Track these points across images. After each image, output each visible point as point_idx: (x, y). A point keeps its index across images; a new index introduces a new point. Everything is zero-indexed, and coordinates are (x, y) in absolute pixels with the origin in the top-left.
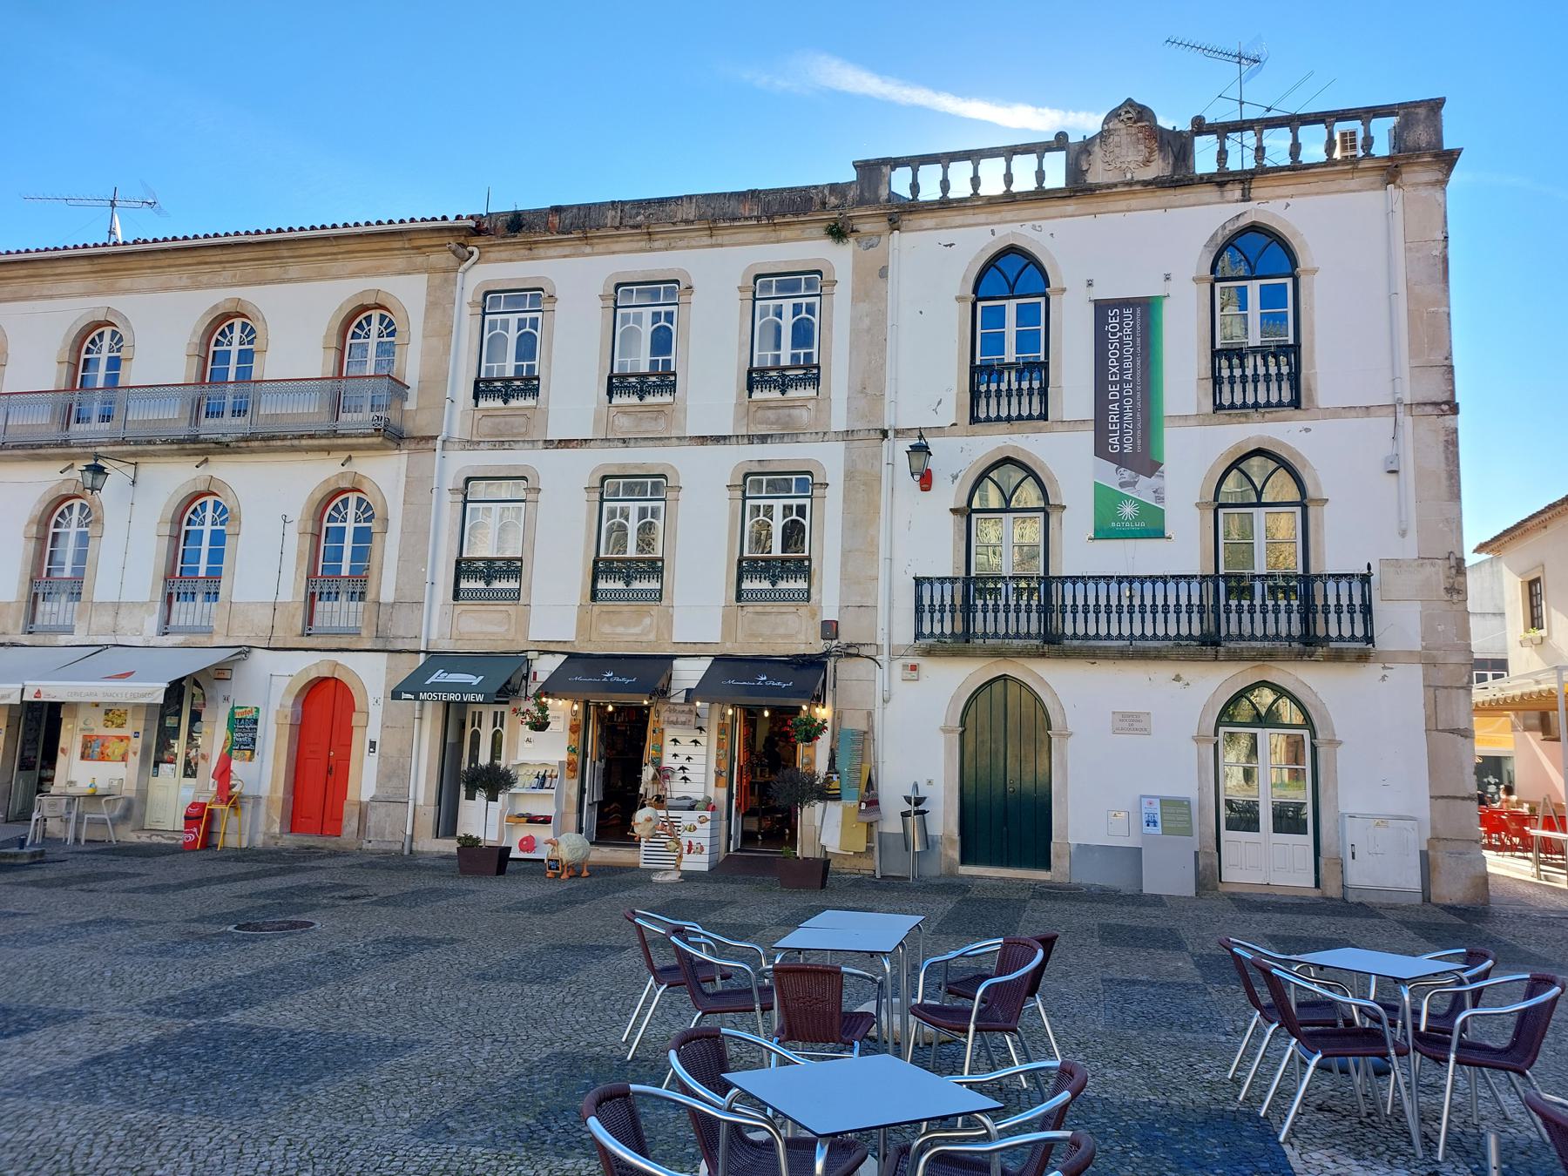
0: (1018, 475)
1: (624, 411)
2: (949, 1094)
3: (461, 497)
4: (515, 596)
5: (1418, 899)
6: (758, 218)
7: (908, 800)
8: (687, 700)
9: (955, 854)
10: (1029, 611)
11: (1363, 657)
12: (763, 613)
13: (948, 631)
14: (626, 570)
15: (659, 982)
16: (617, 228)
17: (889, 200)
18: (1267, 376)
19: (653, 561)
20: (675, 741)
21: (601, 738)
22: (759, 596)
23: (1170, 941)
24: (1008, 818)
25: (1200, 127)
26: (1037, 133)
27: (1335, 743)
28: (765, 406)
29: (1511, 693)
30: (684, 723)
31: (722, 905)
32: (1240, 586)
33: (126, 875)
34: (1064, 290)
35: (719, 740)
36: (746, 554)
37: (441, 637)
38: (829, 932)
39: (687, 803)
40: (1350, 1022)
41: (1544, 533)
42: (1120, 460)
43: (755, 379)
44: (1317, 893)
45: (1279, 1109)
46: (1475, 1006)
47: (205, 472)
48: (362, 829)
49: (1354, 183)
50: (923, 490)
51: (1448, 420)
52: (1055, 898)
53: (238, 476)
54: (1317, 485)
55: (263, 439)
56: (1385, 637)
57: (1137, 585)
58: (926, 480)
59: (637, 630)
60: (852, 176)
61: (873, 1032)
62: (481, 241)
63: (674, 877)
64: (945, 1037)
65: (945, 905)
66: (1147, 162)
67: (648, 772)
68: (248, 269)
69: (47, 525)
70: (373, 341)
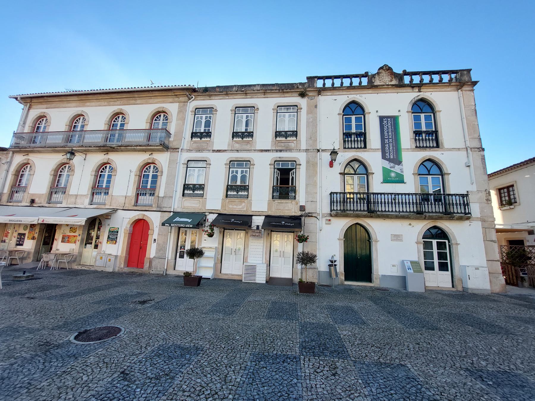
1: (237, 142)
3: (186, 166)
4: (202, 196)
6: (279, 90)
9: (344, 278)
13: (339, 209)
14: (237, 188)
16: (237, 91)
19: (245, 186)
25: (405, 73)
28: (280, 142)
33: (57, 287)
36: (229, 184)
37: (178, 207)
47: (107, 157)
48: (150, 267)
49: (449, 89)
51: (482, 153)
53: (116, 158)
54: (447, 169)
55: (125, 146)
56: (474, 215)
59: (241, 207)
62: (196, 94)
66: (391, 81)
68: (125, 101)
69: (58, 172)
70: (161, 121)
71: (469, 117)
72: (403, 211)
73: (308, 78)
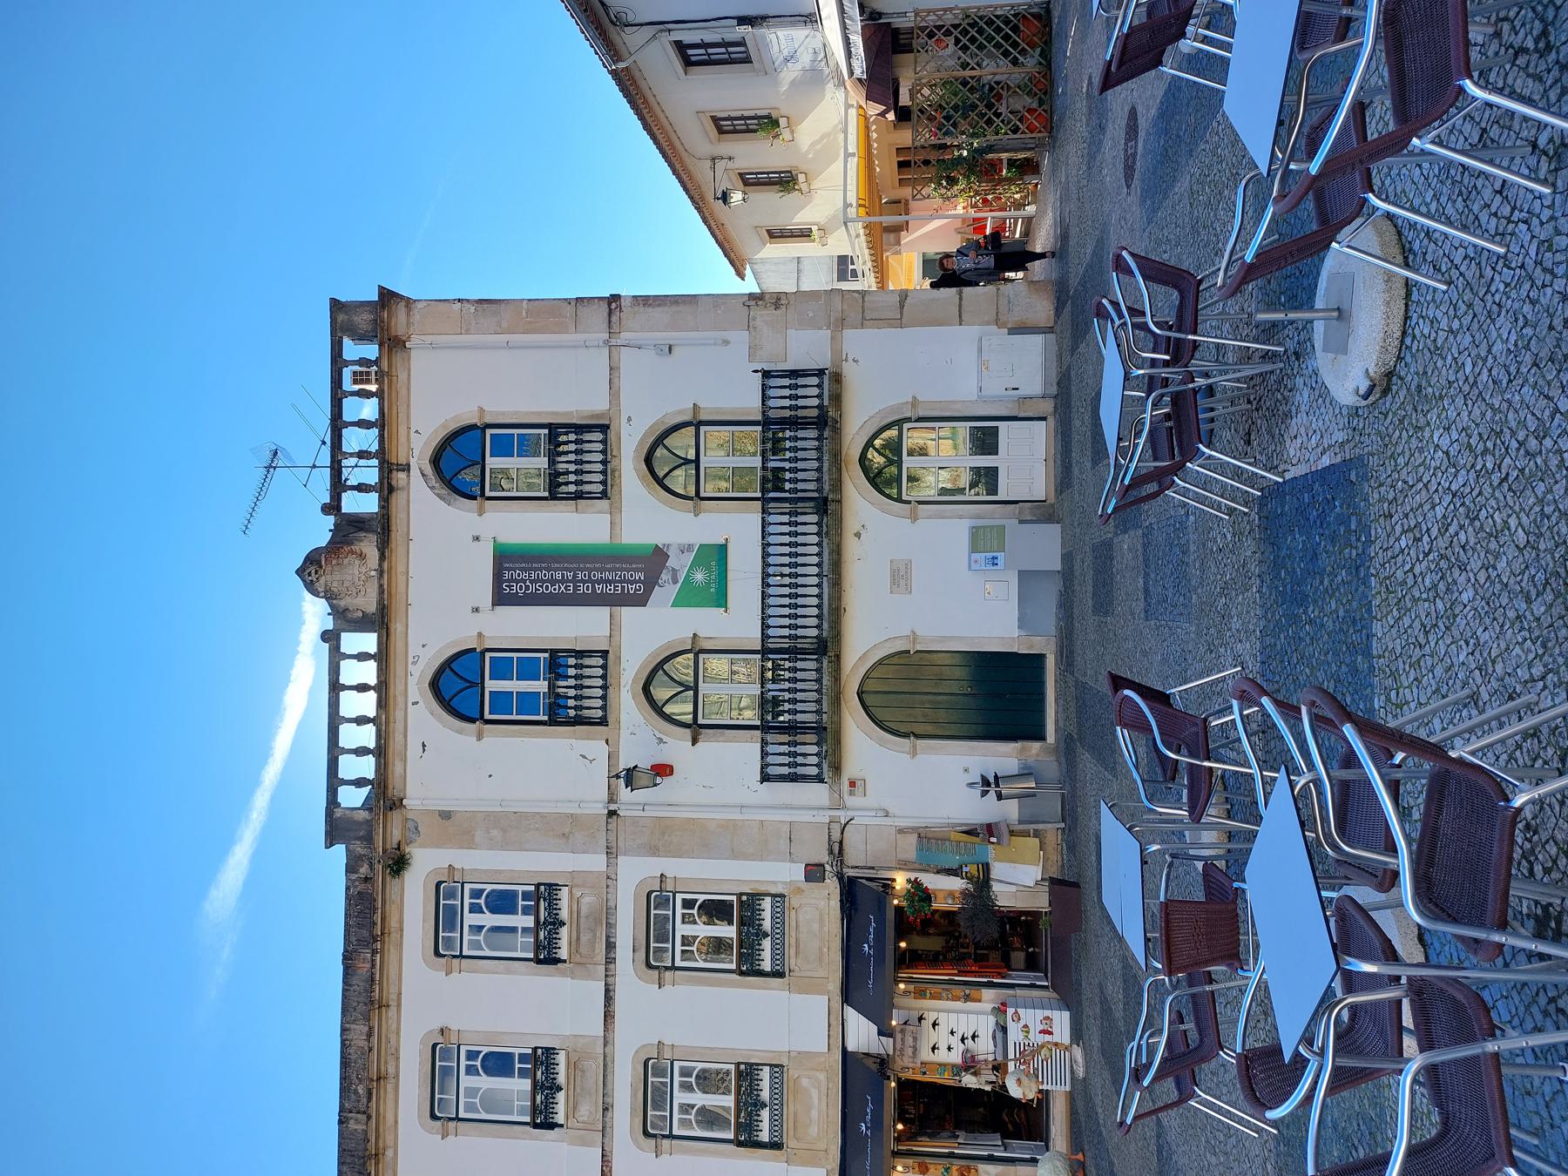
0: (660, 452)
1: (572, 1109)
2: (1278, 815)
5: (1051, 337)
6: (374, 952)
7: (984, 793)
8: (890, 1035)
9: (1035, 746)
10: (796, 670)
11: (837, 378)
12: (797, 946)
13: (814, 749)
15: (1193, 1095)
16: (369, 1117)
17: (370, 810)
18: (576, 452)
19: (739, 1074)
20: (934, 1049)
21: (932, 1136)
22: (779, 953)
23: (1104, 553)
24: (997, 695)
25: (332, 507)
26: (315, 682)
27: (915, 403)
28: (575, 943)
29: (867, 257)
30: (915, 1039)
31: (1104, 1001)
32: (773, 480)
34: (480, 634)
35: (933, 997)
36: (733, 966)
38: (1124, 900)
39: (999, 1035)
40: (1167, 417)
41: (728, 226)
42: (651, 583)
43: (546, 956)
44: (1051, 420)
45: (1252, 480)
46: (1143, 314)
49: (402, 376)
50: (671, 773)
52: (1072, 652)
54: (680, 412)
57: (771, 570)
58: (662, 770)
59: (814, 1093)
60: (340, 850)
61: (1221, 864)
63: (1078, 1052)
64: (1220, 787)
65: (1087, 763)
66: (362, 556)
67: (969, 1081)
71: (505, 325)
72: (819, 565)
73: (330, 843)
